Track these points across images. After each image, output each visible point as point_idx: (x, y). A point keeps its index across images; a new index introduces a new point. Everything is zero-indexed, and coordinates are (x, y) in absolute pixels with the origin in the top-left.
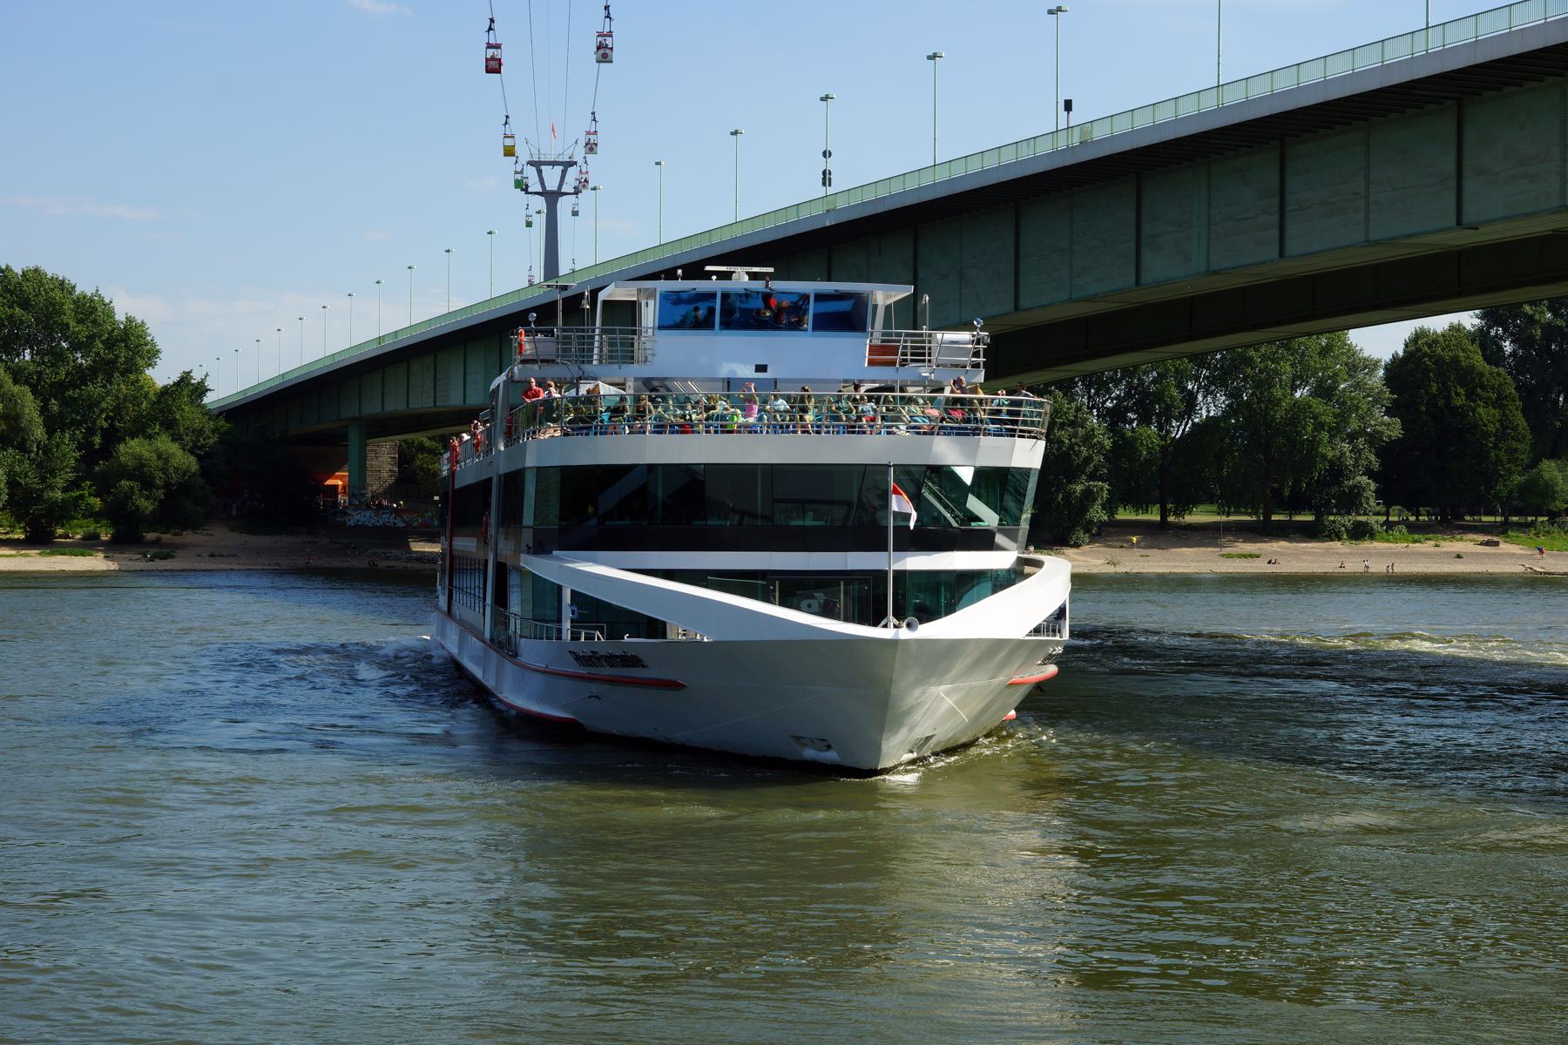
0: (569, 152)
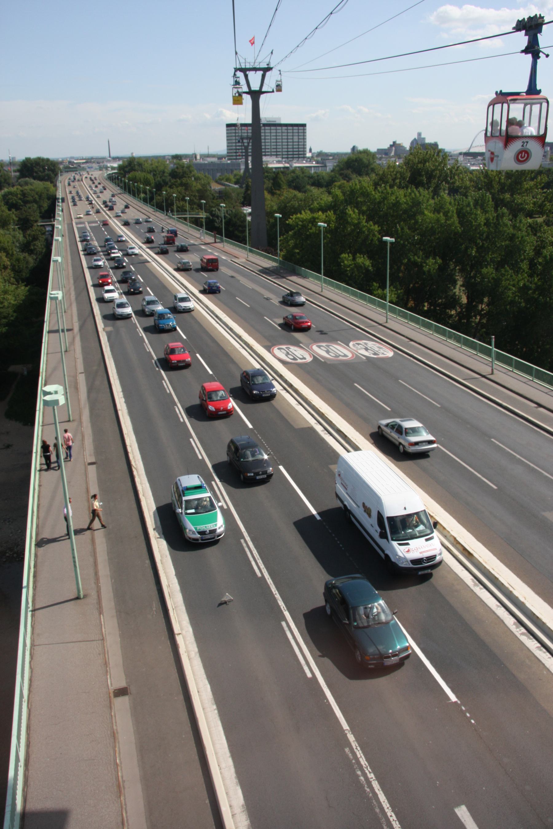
0: (267, 61)
